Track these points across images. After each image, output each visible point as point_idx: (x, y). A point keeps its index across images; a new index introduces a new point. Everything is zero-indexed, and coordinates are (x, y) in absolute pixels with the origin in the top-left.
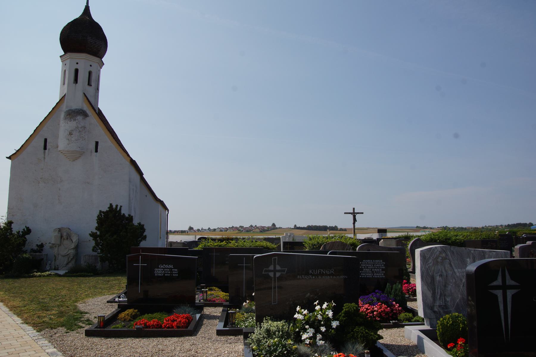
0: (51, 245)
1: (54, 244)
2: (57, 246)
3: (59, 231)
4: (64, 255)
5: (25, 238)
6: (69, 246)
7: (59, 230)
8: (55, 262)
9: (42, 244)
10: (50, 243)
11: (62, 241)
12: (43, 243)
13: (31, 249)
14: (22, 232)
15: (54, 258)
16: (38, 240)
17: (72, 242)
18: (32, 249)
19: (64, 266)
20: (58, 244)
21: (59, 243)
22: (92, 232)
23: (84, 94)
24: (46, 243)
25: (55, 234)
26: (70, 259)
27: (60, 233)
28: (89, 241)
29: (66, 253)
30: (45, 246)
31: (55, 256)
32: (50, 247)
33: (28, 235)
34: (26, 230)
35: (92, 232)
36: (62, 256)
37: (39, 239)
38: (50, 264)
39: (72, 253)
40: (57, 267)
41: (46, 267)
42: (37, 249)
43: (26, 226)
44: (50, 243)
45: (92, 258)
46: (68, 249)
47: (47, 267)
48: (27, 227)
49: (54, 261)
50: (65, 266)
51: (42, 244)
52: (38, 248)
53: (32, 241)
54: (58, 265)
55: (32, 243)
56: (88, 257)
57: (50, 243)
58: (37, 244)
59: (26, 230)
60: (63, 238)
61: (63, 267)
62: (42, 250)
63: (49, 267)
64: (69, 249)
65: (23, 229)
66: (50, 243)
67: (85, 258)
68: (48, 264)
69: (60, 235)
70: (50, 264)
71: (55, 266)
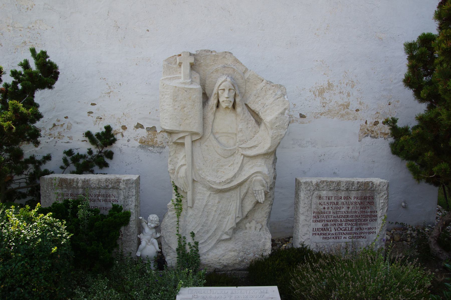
0: (143, 133)
1: (170, 133)
2: (188, 141)
3: (192, 66)
4: (220, 187)
5: (31, 104)
6: (245, 142)
7: (192, 60)
8: (179, 215)
9: (108, 128)
10: (142, 127)
11: (210, 115)
12: (112, 126)
13: (65, 152)
14: (14, 74)
15: (174, 197)
16: (90, 113)
17: (258, 120)
18: (69, 153)
19: (225, 237)
20: (193, 134)
21: (196, 127)
22: (88, 149)
23: (82, 141)
24: (124, 128)
25: (175, 83)
26: (249, 206)
27: (196, 76)
28: (302, 116)
29: (231, 180)
30: (118, 137)
31: (176, 188)
32: (141, 142)
33: (46, 91)
34: (33, 66)
35: (88, 149)
36: (211, 188)
37: (92, 109)
38: (157, 228)
39: (259, 178)
40: (189, 240)
41: (139, 243)
42: (90, 152)
43: (33, 51)
44: (142, 127)
45: (346, 198)
46: (239, 159)
47: (143, 243)
48: (38, 52)
49: (172, 213)
50: (230, 239)
51: (108, 128)
52: (93, 148)
53: (66, 118)
54: (193, 234)
55: (69, 128)
56: (330, 194)
57: (139, 126)
58: (86, 131)
59: (33, 66)
60: (213, 102)
61: (220, 241)
62: (110, 155)
63: (155, 242)
64: (245, 156)
65: (21, 65)
66: (139, 126)
67: (320, 197)
68: (147, 230)
69: (197, 86)
70: (157, 228)
71: (181, 239)
